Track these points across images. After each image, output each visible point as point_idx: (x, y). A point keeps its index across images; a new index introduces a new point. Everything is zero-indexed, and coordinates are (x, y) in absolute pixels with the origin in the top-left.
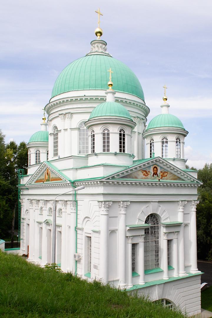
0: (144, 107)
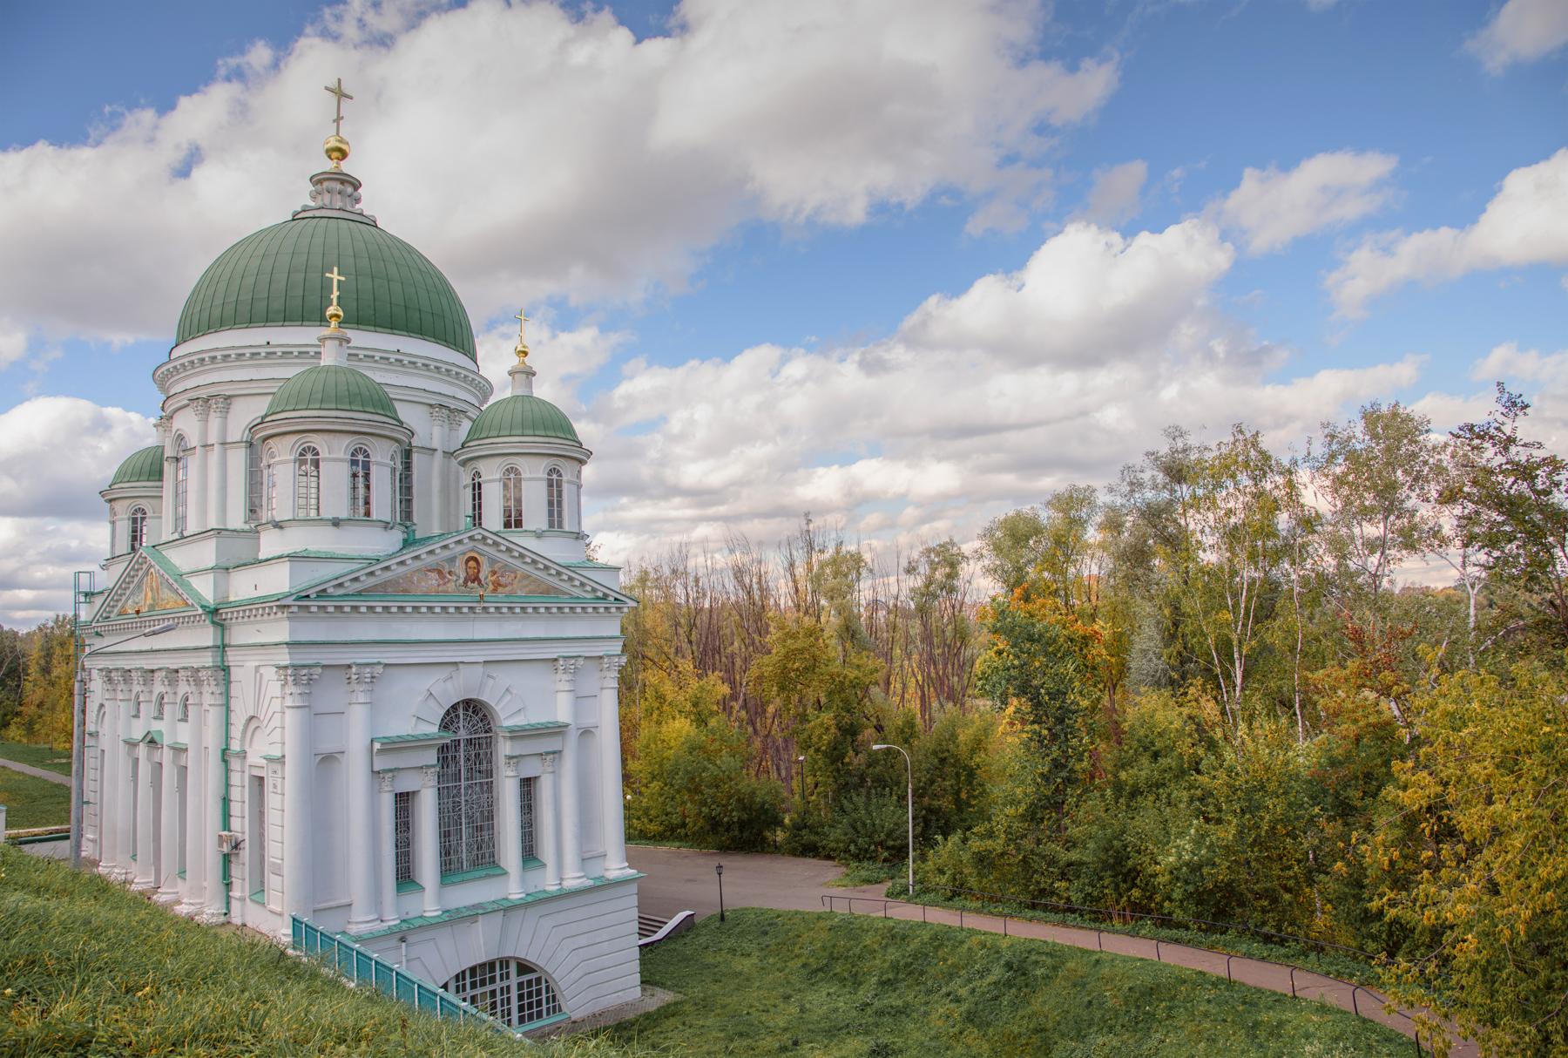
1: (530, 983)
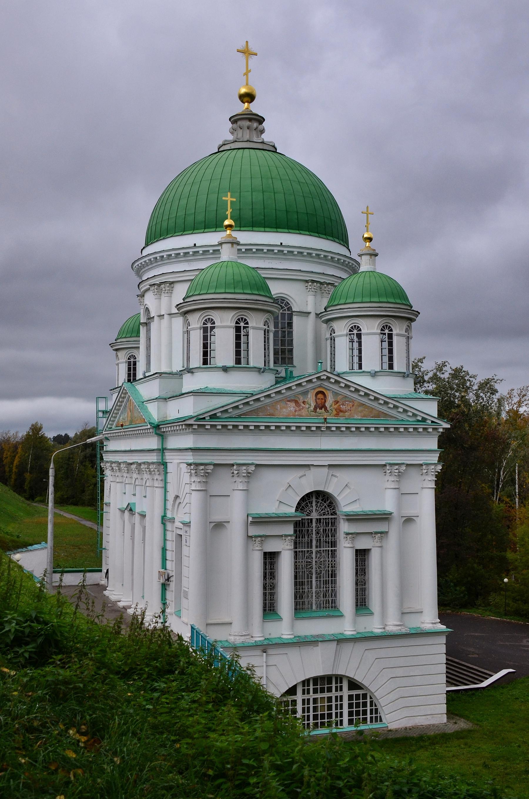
0: (347, 263)
1: (358, 696)
